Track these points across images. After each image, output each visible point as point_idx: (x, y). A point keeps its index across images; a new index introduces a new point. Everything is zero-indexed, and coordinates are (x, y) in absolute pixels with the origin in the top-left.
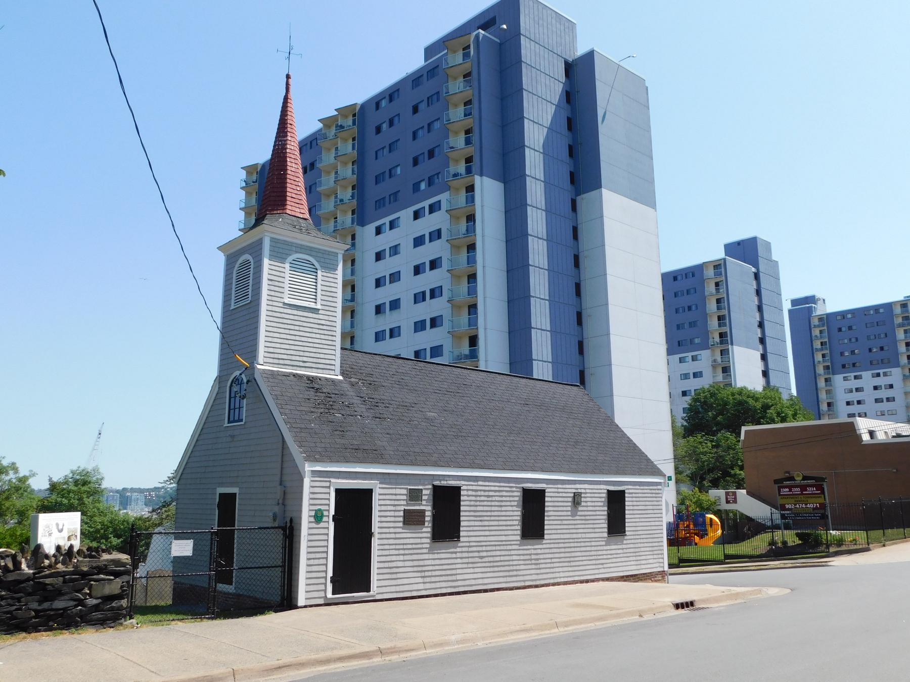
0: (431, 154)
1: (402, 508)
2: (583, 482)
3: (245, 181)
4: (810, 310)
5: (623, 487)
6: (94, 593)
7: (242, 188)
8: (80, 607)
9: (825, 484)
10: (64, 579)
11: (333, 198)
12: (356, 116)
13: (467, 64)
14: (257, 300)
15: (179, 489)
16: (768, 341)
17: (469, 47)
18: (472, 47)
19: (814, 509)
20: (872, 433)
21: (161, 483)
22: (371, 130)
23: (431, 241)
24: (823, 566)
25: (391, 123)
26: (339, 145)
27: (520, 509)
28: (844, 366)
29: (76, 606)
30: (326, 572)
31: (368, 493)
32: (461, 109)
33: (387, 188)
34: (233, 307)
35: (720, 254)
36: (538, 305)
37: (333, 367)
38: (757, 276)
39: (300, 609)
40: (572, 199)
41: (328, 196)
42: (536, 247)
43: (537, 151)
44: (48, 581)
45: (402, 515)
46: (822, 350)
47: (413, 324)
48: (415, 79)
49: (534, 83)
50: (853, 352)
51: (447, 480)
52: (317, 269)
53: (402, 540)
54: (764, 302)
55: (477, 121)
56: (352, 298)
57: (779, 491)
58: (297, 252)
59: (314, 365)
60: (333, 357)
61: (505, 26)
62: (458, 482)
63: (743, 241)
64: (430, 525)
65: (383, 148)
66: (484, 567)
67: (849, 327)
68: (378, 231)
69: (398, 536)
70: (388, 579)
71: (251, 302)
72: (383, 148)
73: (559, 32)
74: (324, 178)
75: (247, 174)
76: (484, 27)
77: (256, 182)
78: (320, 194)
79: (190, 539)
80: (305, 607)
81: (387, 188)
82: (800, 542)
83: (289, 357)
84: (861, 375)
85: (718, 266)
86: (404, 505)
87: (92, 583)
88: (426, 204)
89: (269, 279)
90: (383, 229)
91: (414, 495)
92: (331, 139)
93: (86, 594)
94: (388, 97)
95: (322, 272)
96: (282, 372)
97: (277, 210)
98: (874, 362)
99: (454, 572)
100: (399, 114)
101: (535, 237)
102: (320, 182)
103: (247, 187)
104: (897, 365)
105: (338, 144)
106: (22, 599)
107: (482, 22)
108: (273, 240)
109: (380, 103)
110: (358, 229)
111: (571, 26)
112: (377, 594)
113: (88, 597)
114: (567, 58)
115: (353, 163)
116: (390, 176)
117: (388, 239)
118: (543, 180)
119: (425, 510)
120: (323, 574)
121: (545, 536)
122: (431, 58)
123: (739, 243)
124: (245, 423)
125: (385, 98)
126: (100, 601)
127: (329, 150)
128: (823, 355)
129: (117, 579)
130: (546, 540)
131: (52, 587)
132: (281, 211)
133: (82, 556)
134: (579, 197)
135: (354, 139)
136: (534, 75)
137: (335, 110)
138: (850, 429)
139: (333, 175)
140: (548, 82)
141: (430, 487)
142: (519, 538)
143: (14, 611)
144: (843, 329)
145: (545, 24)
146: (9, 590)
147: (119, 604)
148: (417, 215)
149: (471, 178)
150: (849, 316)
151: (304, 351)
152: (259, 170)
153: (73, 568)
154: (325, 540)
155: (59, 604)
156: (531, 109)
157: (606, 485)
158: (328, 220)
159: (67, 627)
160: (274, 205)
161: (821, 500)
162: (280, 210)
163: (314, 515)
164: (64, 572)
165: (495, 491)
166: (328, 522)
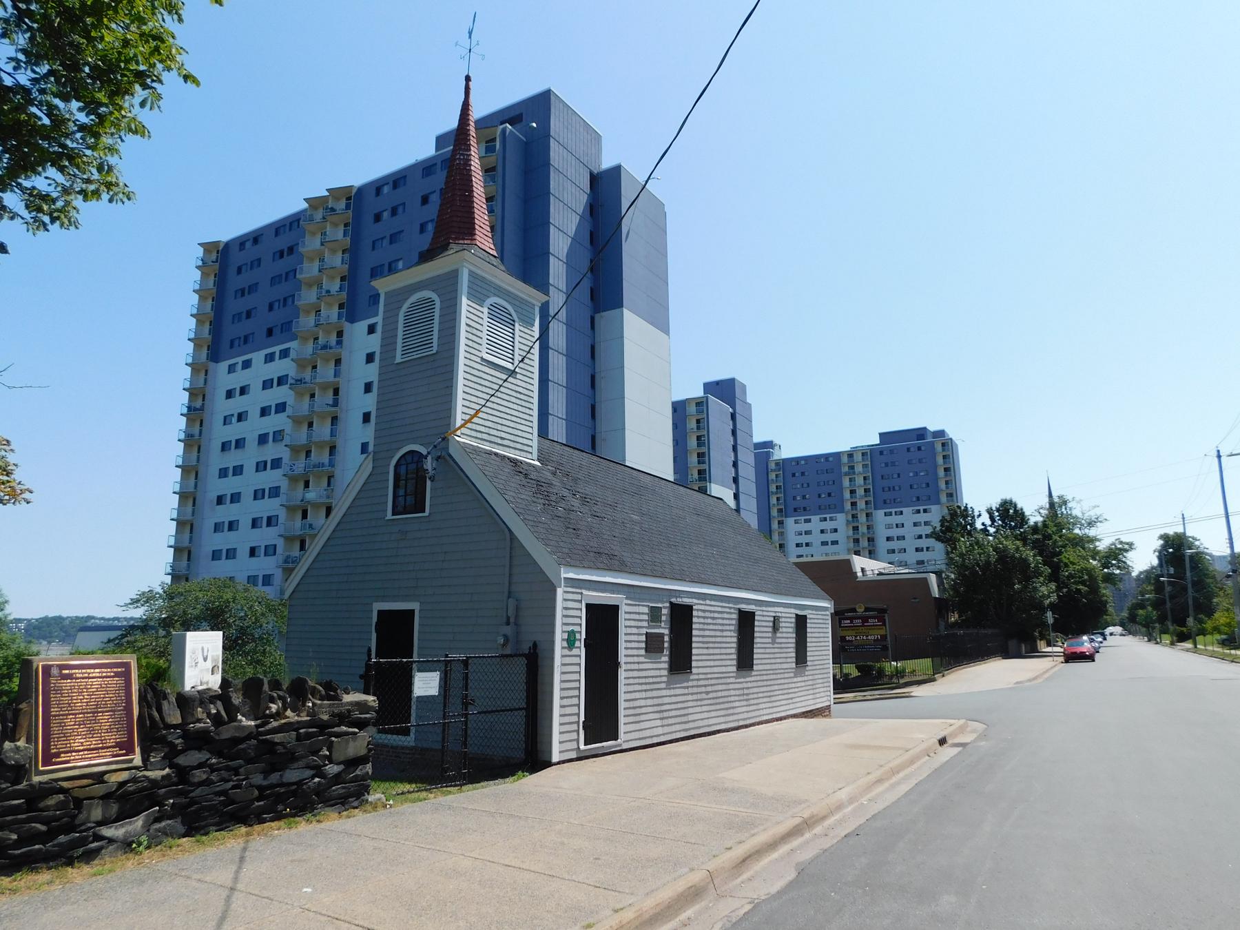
1: (644, 631)
2: (776, 604)
3: (202, 260)
4: (768, 455)
5: (805, 611)
6: (335, 756)
8: (317, 780)
9: (886, 615)
10: (299, 735)
11: (315, 289)
13: (493, 157)
14: (383, 367)
16: (741, 480)
17: (494, 140)
18: (498, 140)
19: (874, 640)
20: (863, 570)
21: (121, 606)
22: (232, 270)
23: (272, 380)
24: (907, 697)
25: (394, 212)
27: (736, 635)
28: (795, 510)
29: (313, 777)
30: (578, 715)
31: (614, 609)
34: (398, 359)
35: (700, 393)
36: (555, 424)
37: (529, 449)
38: (733, 416)
39: (554, 767)
40: (591, 316)
42: (556, 362)
43: (561, 260)
44: (278, 738)
45: (644, 639)
46: (776, 493)
49: (561, 189)
50: (804, 497)
51: (682, 597)
52: (514, 321)
53: (655, 667)
54: (739, 442)
56: (334, 402)
57: (840, 623)
58: (495, 295)
59: (512, 444)
60: (529, 436)
61: (534, 125)
62: (690, 600)
63: (722, 381)
64: (668, 653)
65: (382, 239)
66: (711, 705)
67: (802, 473)
69: (642, 666)
70: (632, 723)
71: (437, 352)
72: (382, 239)
73: (586, 141)
74: (306, 265)
76: (512, 121)
77: (217, 262)
79: (436, 671)
80: (559, 763)
82: (860, 674)
83: (486, 430)
84: (810, 519)
85: (700, 404)
86: (646, 627)
87: (333, 739)
89: (467, 324)
91: (654, 615)
93: (326, 756)
94: (391, 183)
95: (520, 325)
96: (484, 449)
97: (464, 239)
98: (823, 507)
99: (685, 712)
100: (404, 203)
101: (556, 351)
102: (302, 269)
103: (203, 267)
104: (842, 511)
105: (326, 227)
106: (240, 770)
107: (512, 114)
108: (471, 274)
110: (212, 365)
111: (597, 138)
112: (624, 742)
113: (327, 762)
114: (592, 169)
115: (344, 252)
118: (565, 291)
119: (663, 633)
120: (575, 719)
121: (754, 666)
123: (717, 383)
124: (430, 514)
125: (388, 183)
126: (341, 767)
127: (314, 234)
128: (777, 498)
129: (362, 734)
130: (694, 674)
131: (282, 748)
132: (469, 242)
133: (318, 697)
134: (599, 314)
135: (346, 225)
136: (561, 181)
137: (304, 199)
138: (847, 564)
139: (316, 264)
140: (573, 191)
141: (668, 605)
142: (734, 669)
143: (231, 789)
144: (797, 474)
145: (573, 130)
146: (219, 754)
147: (364, 771)
150: (803, 462)
151: (502, 425)
152: (221, 248)
153: (307, 716)
154: (576, 672)
155: (292, 775)
156: (557, 215)
157: (795, 608)
159: (300, 812)
160: (459, 233)
161: (883, 632)
162: (467, 239)
163: (567, 638)
164: (298, 722)
165: (719, 612)
166: (580, 648)
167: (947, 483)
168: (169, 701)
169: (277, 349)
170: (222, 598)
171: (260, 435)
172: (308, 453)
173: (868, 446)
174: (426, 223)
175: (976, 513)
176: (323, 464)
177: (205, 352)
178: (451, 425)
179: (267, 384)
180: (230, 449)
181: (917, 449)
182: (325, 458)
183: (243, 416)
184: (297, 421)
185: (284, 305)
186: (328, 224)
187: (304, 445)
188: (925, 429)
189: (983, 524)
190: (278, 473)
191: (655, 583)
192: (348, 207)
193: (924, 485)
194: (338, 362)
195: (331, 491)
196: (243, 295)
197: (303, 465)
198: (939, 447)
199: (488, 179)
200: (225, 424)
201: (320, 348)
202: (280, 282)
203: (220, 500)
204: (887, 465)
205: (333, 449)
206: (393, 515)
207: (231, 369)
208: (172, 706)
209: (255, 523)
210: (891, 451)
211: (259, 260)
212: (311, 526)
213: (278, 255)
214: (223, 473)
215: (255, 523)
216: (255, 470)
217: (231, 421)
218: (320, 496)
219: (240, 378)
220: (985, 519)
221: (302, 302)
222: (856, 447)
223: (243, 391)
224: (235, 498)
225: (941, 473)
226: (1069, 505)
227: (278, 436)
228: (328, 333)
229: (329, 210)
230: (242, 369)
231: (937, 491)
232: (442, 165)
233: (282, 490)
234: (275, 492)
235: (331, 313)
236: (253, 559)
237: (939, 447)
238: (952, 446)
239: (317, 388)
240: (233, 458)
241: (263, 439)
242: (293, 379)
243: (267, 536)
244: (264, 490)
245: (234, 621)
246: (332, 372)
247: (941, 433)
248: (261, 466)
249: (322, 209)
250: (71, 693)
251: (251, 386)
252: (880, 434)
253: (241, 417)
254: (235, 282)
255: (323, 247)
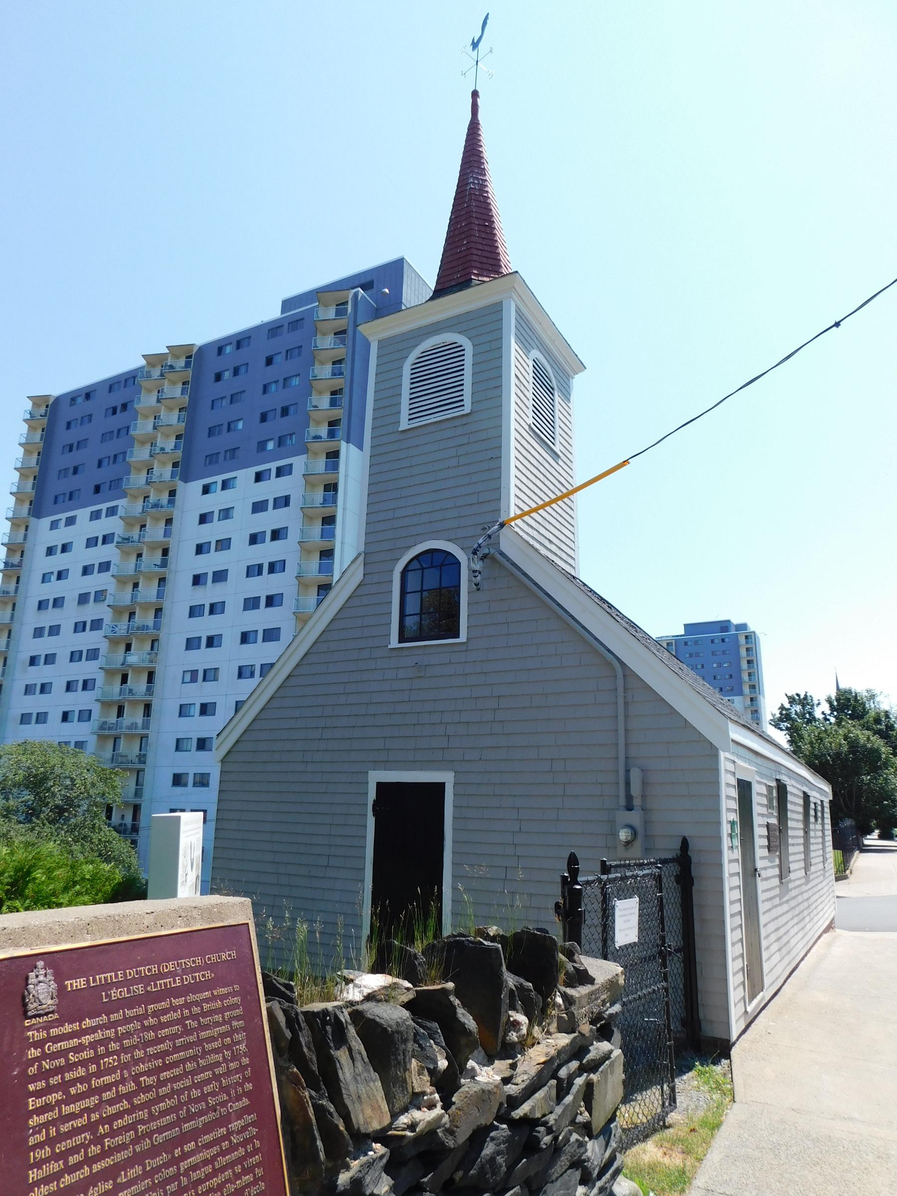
0: (285, 412)
7: (25, 420)
12: (191, 358)
15: (222, 791)
17: (346, 303)
22: (62, 425)
23: (97, 538)
25: (236, 371)
26: (166, 387)
32: (329, 367)
33: (224, 441)
34: (404, 425)
41: (143, 443)
47: (243, 600)
48: (273, 329)
55: (348, 383)
56: (162, 562)
61: (387, 291)
65: (222, 398)
68: (206, 490)
72: (222, 398)
74: (140, 421)
75: (33, 405)
76: (367, 286)
77: (45, 416)
78: (133, 439)
81: (224, 441)
88: (273, 466)
90: (213, 488)
92: (155, 379)
94: (235, 343)
100: (247, 364)
103: (31, 420)
107: (363, 281)
109: (223, 349)
110: (33, 521)
115: (181, 410)
116: (229, 430)
117: (217, 501)
122: (290, 311)
127: (149, 391)
137: (142, 356)
148: (259, 477)
149: (337, 442)
152: (50, 403)
158: (139, 470)
167: (750, 675)
168: (350, 1050)
169: (104, 507)
170: (49, 763)
171: (80, 595)
172: (132, 615)
173: (673, 636)
174: (269, 384)
175: (816, 702)
176: (147, 626)
177: (26, 506)
178: (502, 511)
179: (91, 542)
180: (47, 608)
181: (721, 641)
182: (150, 620)
183: (64, 574)
184: (121, 580)
185: (114, 462)
186: (166, 382)
187: (128, 606)
188: (729, 621)
189: (823, 713)
190: (98, 635)
191: (771, 753)
192: (188, 365)
193: (727, 677)
194: (169, 522)
195: (154, 655)
196: (71, 450)
197: (126, 627)
198: (742, 640)
199: (338, 341)
200: (43, 582)
201: (150, 506)
202: (111, 439)
203: (33, 661)
204: (691, 655)
205: (158, 611)
206: (400, 642)
207: (54, 525)
208: (359, 1065)
209: (69, 687)
210: (696, 642)
211: (91, 415)
212: (131, 691)
213: (111, 411)
214: (38, 633)
215: (69, 687)
216: (73, 631)
217: (50, 579)
218: (143, 660)
219: (62, 535)
220: (825, 707)
221: (133, 459)
222: (662, 637)
223: (65, 548)
224: (50, 659)
225: (744, 665)
226: (877, 699)
227: (100, 596)
228: (159, 491)
229: (167, 368)
230: (65, 526)
231: (740, 682)
232: (289, 326)
233: (101, 653)
234: (93, 654)
235: (165, 472)
236: (65, 724)
237: (742, 640)
238: (755, 638)
239: (145, 548)
240: (49, 618)
241: (83, 599)
242: (120, 537)
243: (80, 700)
244: (81, 652)
245: (59, 791)
246: (162, 532)
247: (743, 627)
248: (80, 627)
249: (160, 366)
250: (99, 1074)
251: (74, 543)
252: (685, 625)
253: (60, 575)
254: (64, 437)
255: (159, 404)
